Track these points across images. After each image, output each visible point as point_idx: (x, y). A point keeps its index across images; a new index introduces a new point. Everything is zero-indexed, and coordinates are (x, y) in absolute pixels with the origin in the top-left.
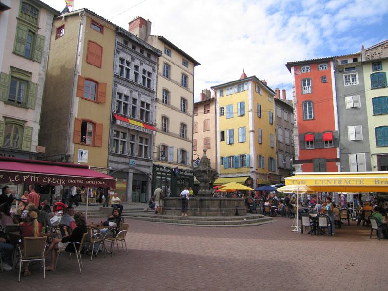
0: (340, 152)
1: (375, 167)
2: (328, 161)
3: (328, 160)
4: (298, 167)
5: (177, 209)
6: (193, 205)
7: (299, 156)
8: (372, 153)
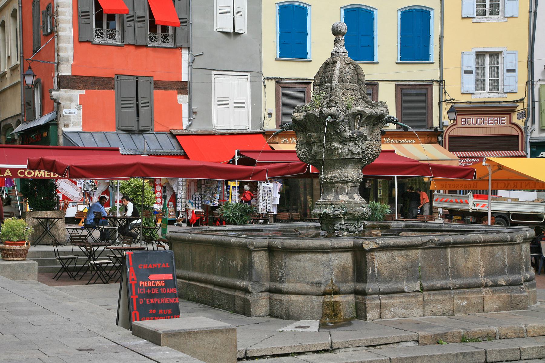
0: (191, 63)
1: (270, 115)
2: (160, 88)
3: (159, 85)
4: (70, 100)
5: (432, 289)
6: (500, 264)
7: (72, 61)
8: (266, 74)
